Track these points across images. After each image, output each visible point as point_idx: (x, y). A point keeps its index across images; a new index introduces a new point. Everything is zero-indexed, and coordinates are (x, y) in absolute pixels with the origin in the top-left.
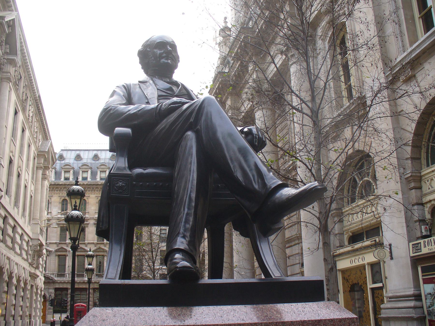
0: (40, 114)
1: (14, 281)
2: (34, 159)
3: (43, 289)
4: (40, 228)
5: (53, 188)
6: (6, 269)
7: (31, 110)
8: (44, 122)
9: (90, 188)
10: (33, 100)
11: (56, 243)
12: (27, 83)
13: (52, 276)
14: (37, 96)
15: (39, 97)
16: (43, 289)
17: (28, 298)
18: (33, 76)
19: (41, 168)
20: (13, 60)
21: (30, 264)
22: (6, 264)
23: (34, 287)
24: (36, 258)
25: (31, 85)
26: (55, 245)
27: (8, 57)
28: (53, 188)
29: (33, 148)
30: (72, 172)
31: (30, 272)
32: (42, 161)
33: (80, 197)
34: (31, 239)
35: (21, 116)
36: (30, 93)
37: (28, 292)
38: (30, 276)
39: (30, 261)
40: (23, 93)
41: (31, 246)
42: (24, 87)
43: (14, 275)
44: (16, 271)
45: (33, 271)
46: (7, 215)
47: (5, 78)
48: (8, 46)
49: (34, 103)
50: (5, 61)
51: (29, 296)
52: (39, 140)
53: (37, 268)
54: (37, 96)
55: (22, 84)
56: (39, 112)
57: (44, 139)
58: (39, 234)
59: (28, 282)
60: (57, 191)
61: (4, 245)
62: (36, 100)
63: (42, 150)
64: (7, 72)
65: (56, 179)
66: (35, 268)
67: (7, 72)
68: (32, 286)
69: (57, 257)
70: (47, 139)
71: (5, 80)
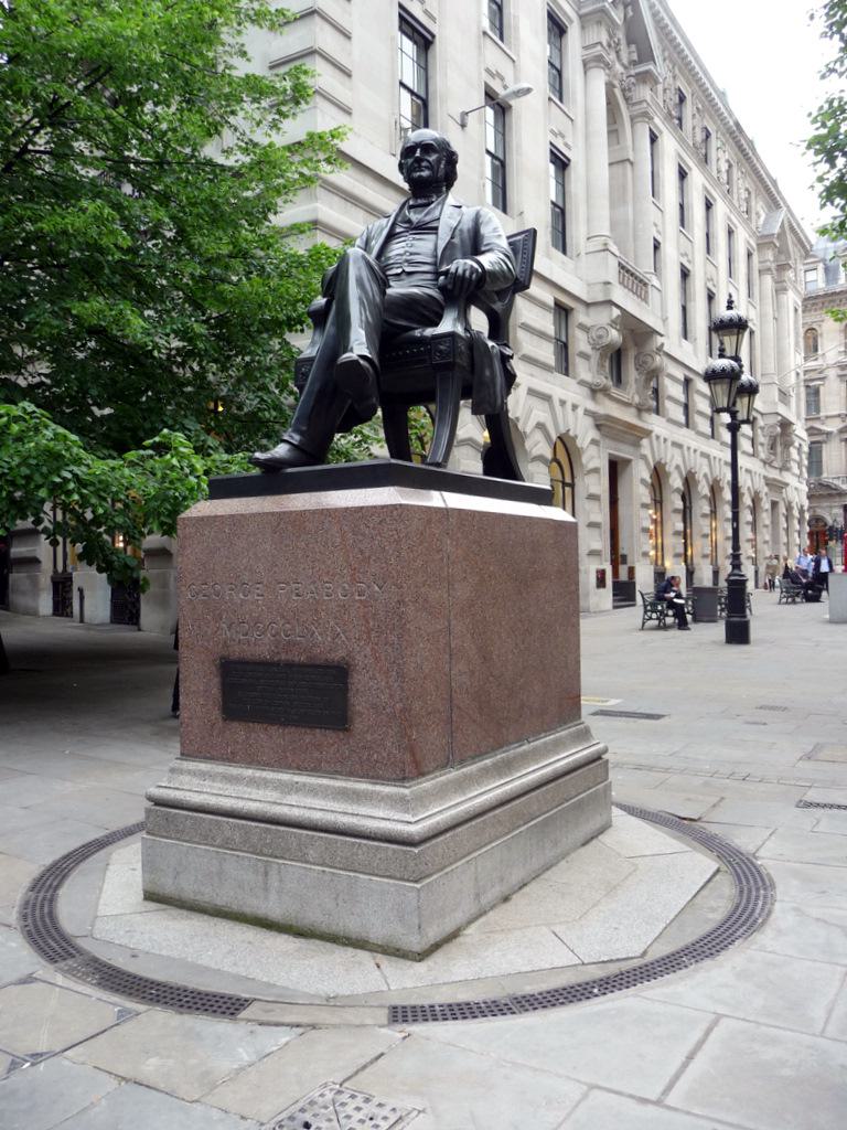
0: (748, 159)
1: (796, 513)
2: (749, 255)
3: (806, 508)
4: (780, 390)
5: (823, 303)
6: (701, 475)
7: (721, 155)
8: (762, 172)
9: (833, 301)
10: (724, 135)
11: (839, 416)
12: (700, 106)
13: (836, 482)
14: (731, 123)
15: (737, 124)
16: (806, 508)
17: (766, 526)
18: (712, 85)
19: (769, 269)
20: (648, 72)
21: (765, 463)
22: (701, 466)
23: (782, 509)
24: (779, 449)
25: (711, 105)
26: (838, 420)
27: (637, 70)
28: (823, 303)
29: (742, 236)
30: (821, 266)
31: (765, 477)
32: (770, 255)
33: (736, 330)
34: (762, 414)
35: (696, 177)
36: (715, 123)
37: (764, 515)
38: (767, 484)
39: (763, 456)
40: (694, 128)
41: (762, 428)
42: (694, 115)
43: (794, 505)
44: (797, 499)
45: (774, 474)
46: (691, 376)
47: (637, 116)
48: (633, 47)
49: (727, 141)
50: (633, 80)
51: (768, 522)
52: (757, 214)
53: (785, 468)
54: (731, 123)
55: (689, 109)
56: (746, 155)
57: (770, 208)
58: (776, 404)
59: (762, 495)
60: (816, 310)
61: (693, 432)
62: (732, 133)
63: (766, 233)
64: (641, 102)
65: (828, 282)
66: (781, 470)
67: (641, 102)
68: (774, 504)
69: (843, 443)
70: (778, 206)
71: (640, 119)
